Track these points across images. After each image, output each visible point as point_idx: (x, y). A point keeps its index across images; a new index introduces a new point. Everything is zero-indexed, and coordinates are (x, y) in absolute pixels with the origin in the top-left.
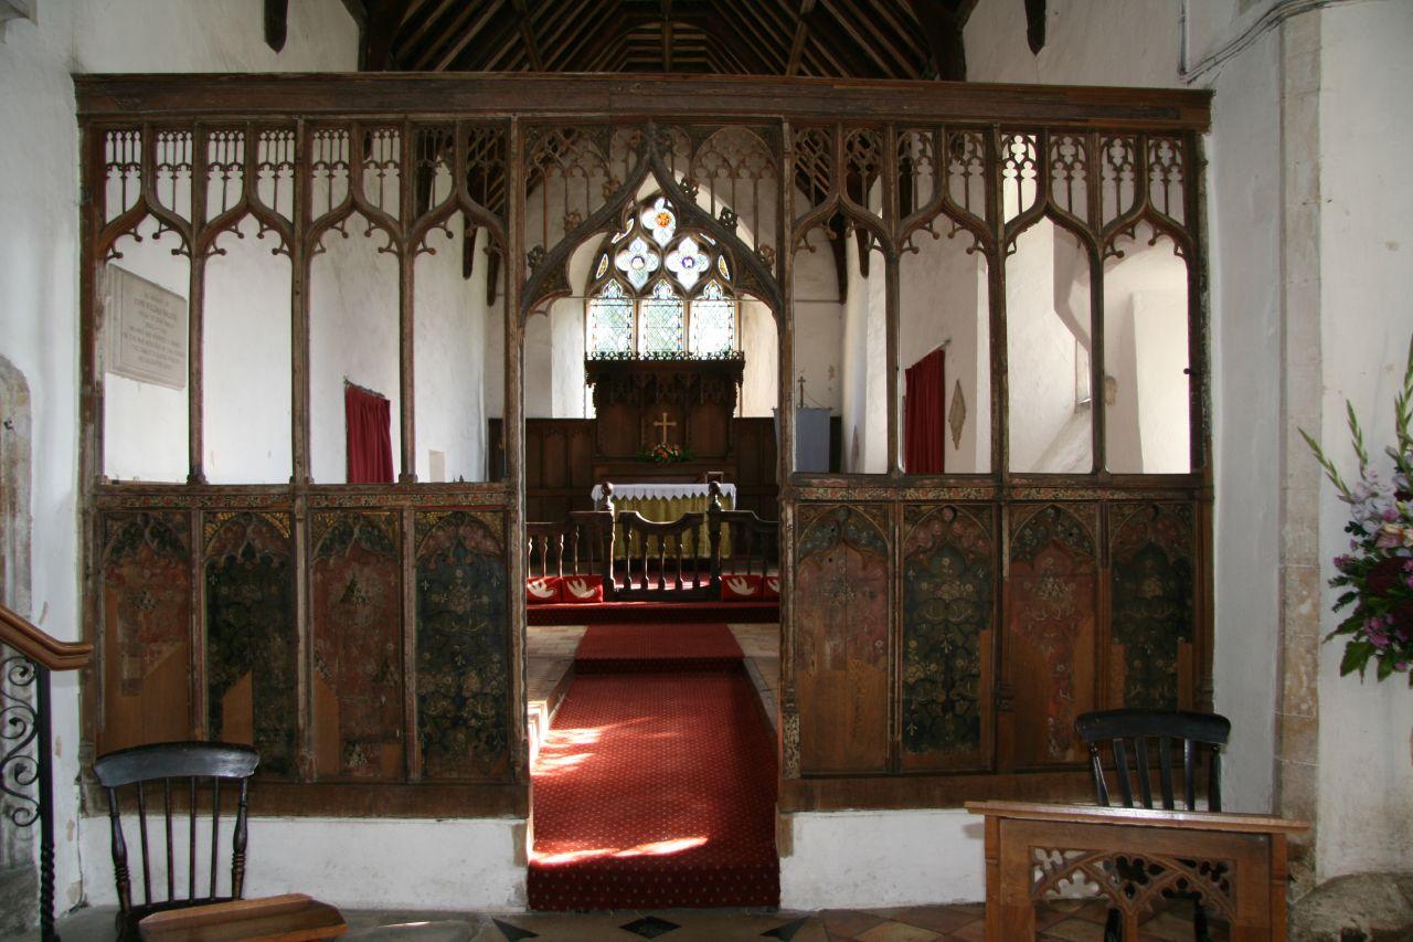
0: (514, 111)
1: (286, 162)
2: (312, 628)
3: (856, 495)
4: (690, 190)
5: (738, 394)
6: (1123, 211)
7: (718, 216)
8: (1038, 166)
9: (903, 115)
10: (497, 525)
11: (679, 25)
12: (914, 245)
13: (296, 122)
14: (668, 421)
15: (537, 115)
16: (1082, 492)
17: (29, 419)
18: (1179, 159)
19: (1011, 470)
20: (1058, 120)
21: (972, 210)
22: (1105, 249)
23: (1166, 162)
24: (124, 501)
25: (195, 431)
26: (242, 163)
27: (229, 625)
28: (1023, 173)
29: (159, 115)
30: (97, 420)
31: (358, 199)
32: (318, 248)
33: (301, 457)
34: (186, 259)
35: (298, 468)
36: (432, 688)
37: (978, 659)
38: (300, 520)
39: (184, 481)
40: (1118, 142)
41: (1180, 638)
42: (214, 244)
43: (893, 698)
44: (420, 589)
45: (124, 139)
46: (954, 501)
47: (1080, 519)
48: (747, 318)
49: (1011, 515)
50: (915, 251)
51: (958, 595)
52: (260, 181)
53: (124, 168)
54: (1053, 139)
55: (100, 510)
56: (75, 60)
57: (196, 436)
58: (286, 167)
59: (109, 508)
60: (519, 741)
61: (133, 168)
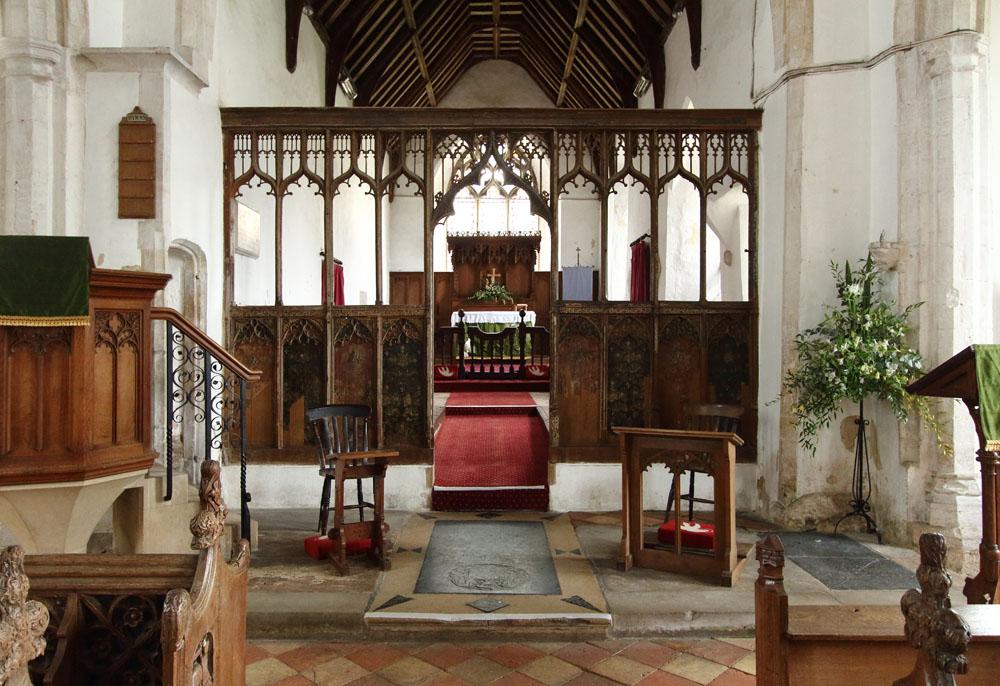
2: (333, 374)
3: (586, 311)
6: (717, 171)
8: (676, 149)
10: (419, 325)
11: (502, 29)
14: (496, 273)
17: (206, 274)
21: (643, 172)
23: (740, 145)
40: (739, 136)
44: (384, 356)
45: (243, 138)
49: (659, 321)
53: (243, 152)
54: (684, 135)
56: (220, 101)
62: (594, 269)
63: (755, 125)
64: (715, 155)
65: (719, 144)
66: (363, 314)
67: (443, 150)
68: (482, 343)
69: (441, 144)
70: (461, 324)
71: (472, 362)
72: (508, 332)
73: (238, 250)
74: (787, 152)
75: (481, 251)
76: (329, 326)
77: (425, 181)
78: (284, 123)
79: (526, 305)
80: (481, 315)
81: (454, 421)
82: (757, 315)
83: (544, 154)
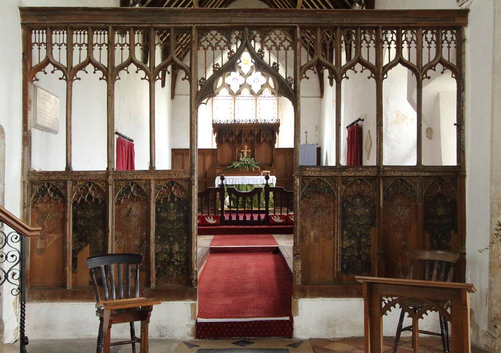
0: (194, 24)
1: (104, 43)
3: (323, 174)
4: (261, 56)
5: (277, 138)
7: (271, 65)
8: (397, 43)
9: (344, 24)
10: (185, 185)
12: (347, 76)
13: (108, 27)
15: (203, 25)
16: (412, 173)
18: (455, 38)
19: (384, 164)
20: (405, 24)
21: (370, 61)
22: (423, 76)
23: (449, 39)
24: (40, 177)
25: (69, 150)
26: (87, 43)
27: (81, 226)
28: (391, 46)
29: (54, 23)
30: (29, 145)
31: (133, 58)
32: (117, 78)
33: (109, 161)
34: (65, 82)
35: (110, 164)
36: (160, 250)
37: (370, 239)
38: (110, 184)
39: (64, 169)
40: (429, 32)
41: (452, 232)
42: (76, 75)
43: (337, 254)
44: (156, 211)
45: (39, 33)
46: (361, 176)
47: (411, 184)
48: (281, 104)
49: (384, 182)
50: (347, 78)
51: (363, 213)
52: (94, 51)
53: (39, 45)
54: (403, 31)
55: (30, 181)
57: (69, 152)
58: (104, 45)
59: (34, 180)
60: (194, 270)
61: (43, 45)
62: (317, 146)
63: (463, 22)
64: (429, 47)
65: (432, 38)
66: (139, 177)
67: (206, 44)
68: (238, 199)
69: (204, 38)
70: (222, 185)
71: (230, 212)
72: (257, 191)
73: (37, 126)
74: (494, 41)
75: (237, 134)
76: (110, 187)
77: (190, 68)
78: (73, 19)
79: (269, 171)
80: (233, 179)
81: (216, 258)
82: (464, 176)
83: (288, 46)
